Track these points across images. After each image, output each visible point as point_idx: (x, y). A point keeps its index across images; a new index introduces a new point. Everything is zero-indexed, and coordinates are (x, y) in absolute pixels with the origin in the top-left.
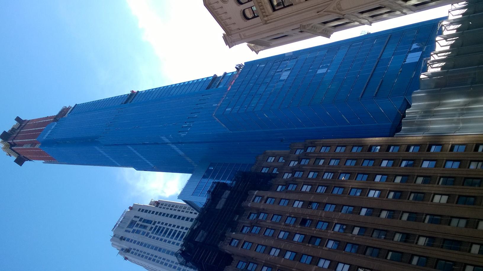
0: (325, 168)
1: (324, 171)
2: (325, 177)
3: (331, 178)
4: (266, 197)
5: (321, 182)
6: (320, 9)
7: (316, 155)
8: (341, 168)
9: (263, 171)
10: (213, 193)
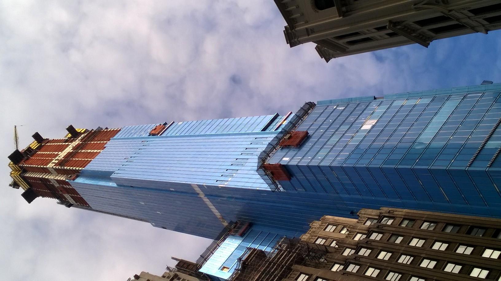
0: (403, 248)
1: (401, 252)
2: (400, 261)
3: (409, 263)
4: (314, 277)
5: (395, 266)
7: (394, 229)
8: (425, 252)
9: (318, 242)
10: (244, 263)
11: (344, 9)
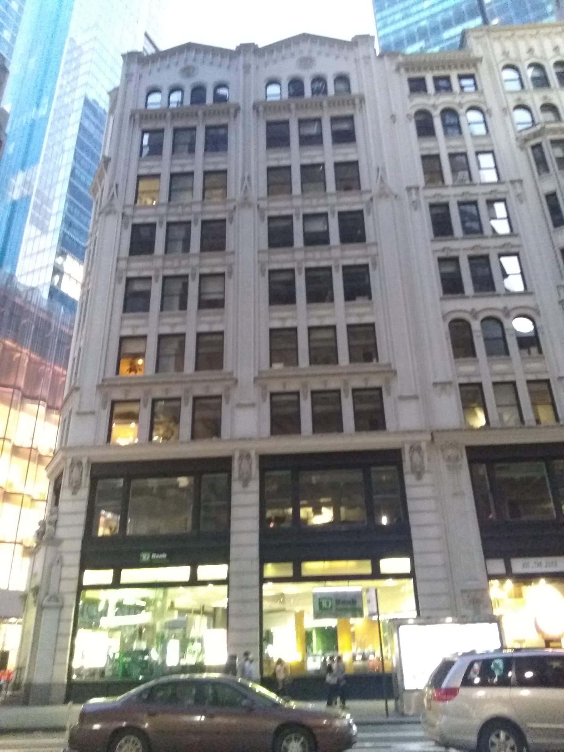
6: (120, 188)
11: (137, 116)
